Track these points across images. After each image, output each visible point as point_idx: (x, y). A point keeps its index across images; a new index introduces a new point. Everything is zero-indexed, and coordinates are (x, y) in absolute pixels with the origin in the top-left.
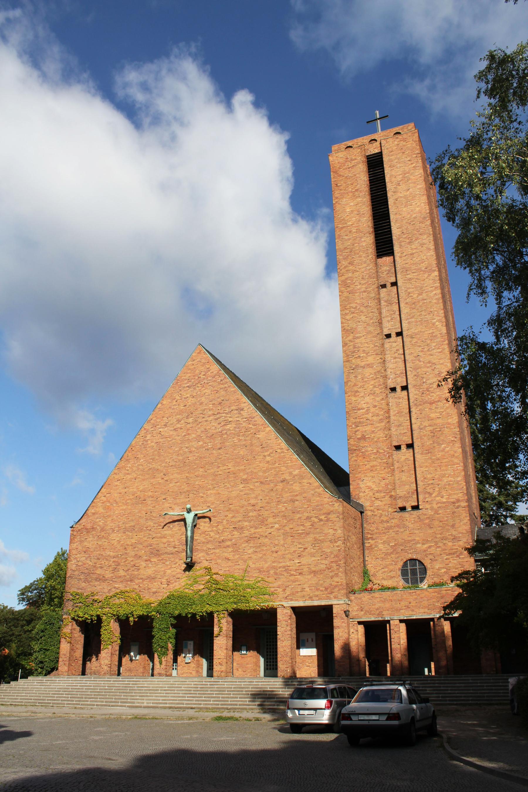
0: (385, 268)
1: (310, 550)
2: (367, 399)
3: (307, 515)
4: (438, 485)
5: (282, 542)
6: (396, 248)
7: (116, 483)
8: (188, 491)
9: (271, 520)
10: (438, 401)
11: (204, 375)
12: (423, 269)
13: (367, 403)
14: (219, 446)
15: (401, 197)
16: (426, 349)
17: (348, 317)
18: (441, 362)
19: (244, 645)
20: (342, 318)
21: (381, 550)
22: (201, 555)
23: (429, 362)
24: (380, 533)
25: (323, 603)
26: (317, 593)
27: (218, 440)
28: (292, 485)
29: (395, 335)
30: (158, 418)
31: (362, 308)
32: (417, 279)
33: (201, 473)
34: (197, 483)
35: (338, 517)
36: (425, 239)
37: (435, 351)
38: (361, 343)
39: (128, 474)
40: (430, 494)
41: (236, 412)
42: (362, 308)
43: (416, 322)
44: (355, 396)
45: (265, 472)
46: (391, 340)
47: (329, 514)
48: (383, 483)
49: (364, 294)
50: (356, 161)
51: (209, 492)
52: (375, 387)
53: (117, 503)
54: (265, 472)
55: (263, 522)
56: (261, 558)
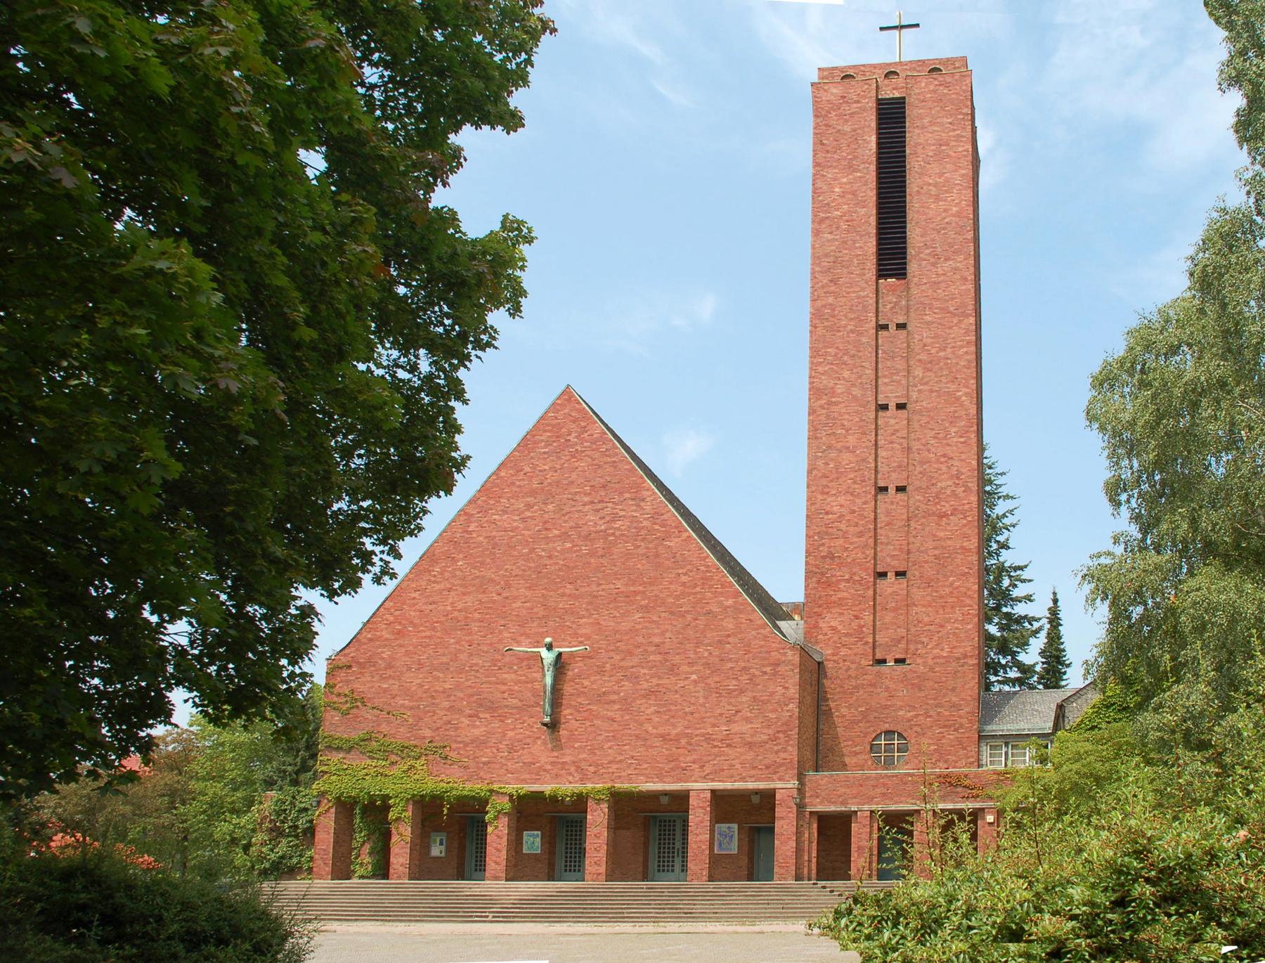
2: (841, 499)
3: (743, 664)
5: (702, 700)
6: (912, 267)
7: (413, 595)
8: (544, 617)
9: (685, 668)
13: (841, 506)
15: (930, 184)
17: (820, 369)
18: (963, 457)
20: (811, 369)
21: (843, 716)
23: (944, 456)
24: (844, 692)
25: (762, 785)
26: (752, 772)
27: (599, 544)
28: (722, 620)
33: (568, 591)
34: (561, 606)
38: (840, 414)
41: (631, 502)
43: (932, 391)
44: (823, 493)
45: (677, 598)
46: (888, 413)
47: (778, 665)
48: (855, 625)
51: (582, 621)
52: (855, 483)
53: (415, 626)
54: (677, 598)
55: (673, 669)
56: (668, 720)
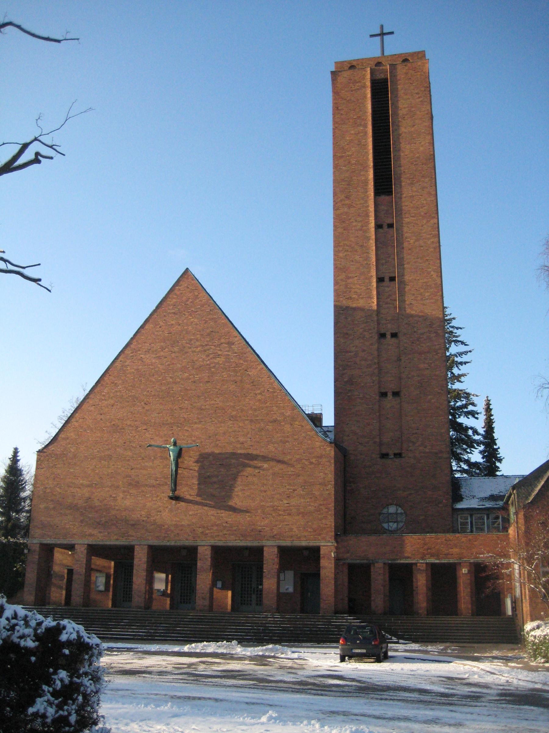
0: (383, 207)
1: (300, 491)
3: (298, 457)
4: (422, 435)
10: (428, 352)
11: (191, 302)
12: (422, 214)
13: (356, 346)
14: (207, 380)
16: (419, 298)
19: (220, 580)
22: (185, 489)
29: (388, 280)
30: (139, 344)
31: (357, 247)
32: (415, 223)
35: (329, 461)
36: (426, 183)
37: (428, 301)
39: (105, 400)
40: (414, 443)
42: (357, 247)
49: (359, 232)
50: (360, 84)
53: (92, 430)
